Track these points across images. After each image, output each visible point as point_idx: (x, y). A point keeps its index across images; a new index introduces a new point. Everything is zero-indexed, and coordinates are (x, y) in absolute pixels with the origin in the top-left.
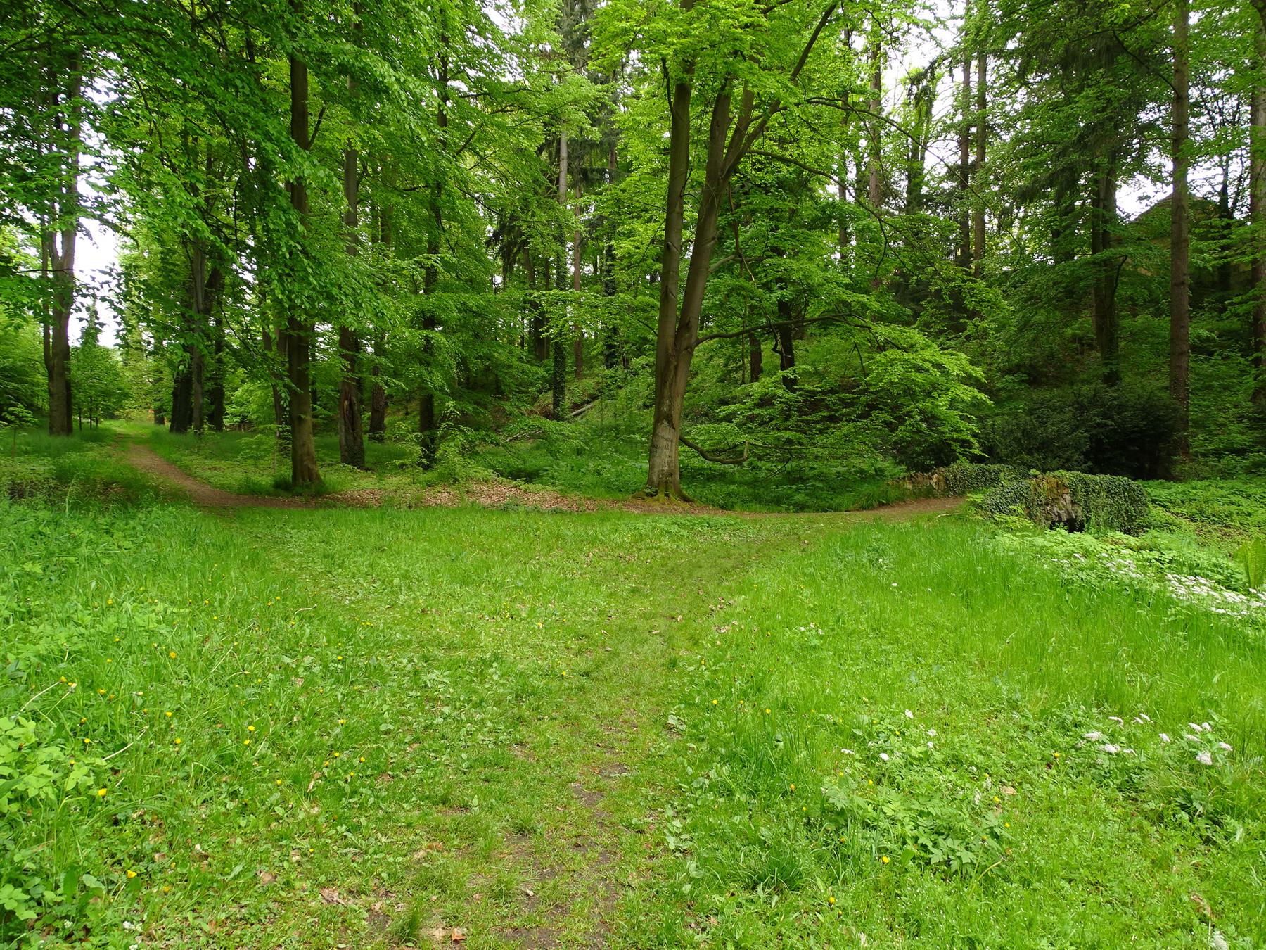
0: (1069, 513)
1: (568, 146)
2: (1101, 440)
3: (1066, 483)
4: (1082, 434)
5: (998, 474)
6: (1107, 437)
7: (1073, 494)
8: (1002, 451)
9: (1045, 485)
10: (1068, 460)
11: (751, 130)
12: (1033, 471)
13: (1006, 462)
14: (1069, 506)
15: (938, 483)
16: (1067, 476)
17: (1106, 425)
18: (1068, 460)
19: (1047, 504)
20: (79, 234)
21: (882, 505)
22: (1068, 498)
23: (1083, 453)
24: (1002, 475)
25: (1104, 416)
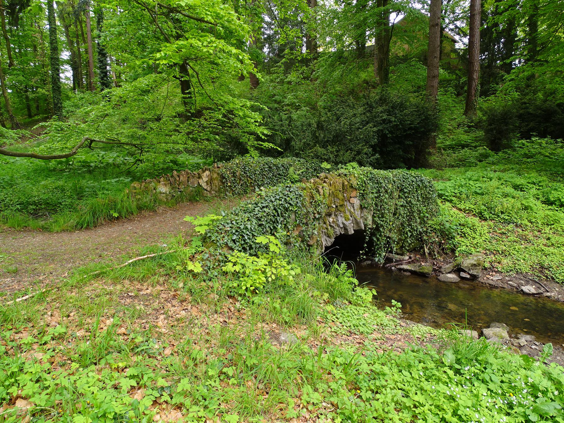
0: (357, 223)
1: (481, 37)
2: (385, 135)
3: (354, 182)
4: (371, 129)
5: (287, 169)
6: (391, 132)
7: (363, 197)
8: (297, 144)
9: (326, 189)
10: (359, 153)
11: (17, 10)
12: (325, 165)
13: (297, 155)
14: (358, 213)
15: (210, 181)
16: (355, 172)
17: (390, 122)
18: (359, 153)
19: (329, 215)
20: (467, 44)
21: (112, 220)
22: (356, 202)
23: (371, 146)
24: (292, 169)
25: (389, 113)
